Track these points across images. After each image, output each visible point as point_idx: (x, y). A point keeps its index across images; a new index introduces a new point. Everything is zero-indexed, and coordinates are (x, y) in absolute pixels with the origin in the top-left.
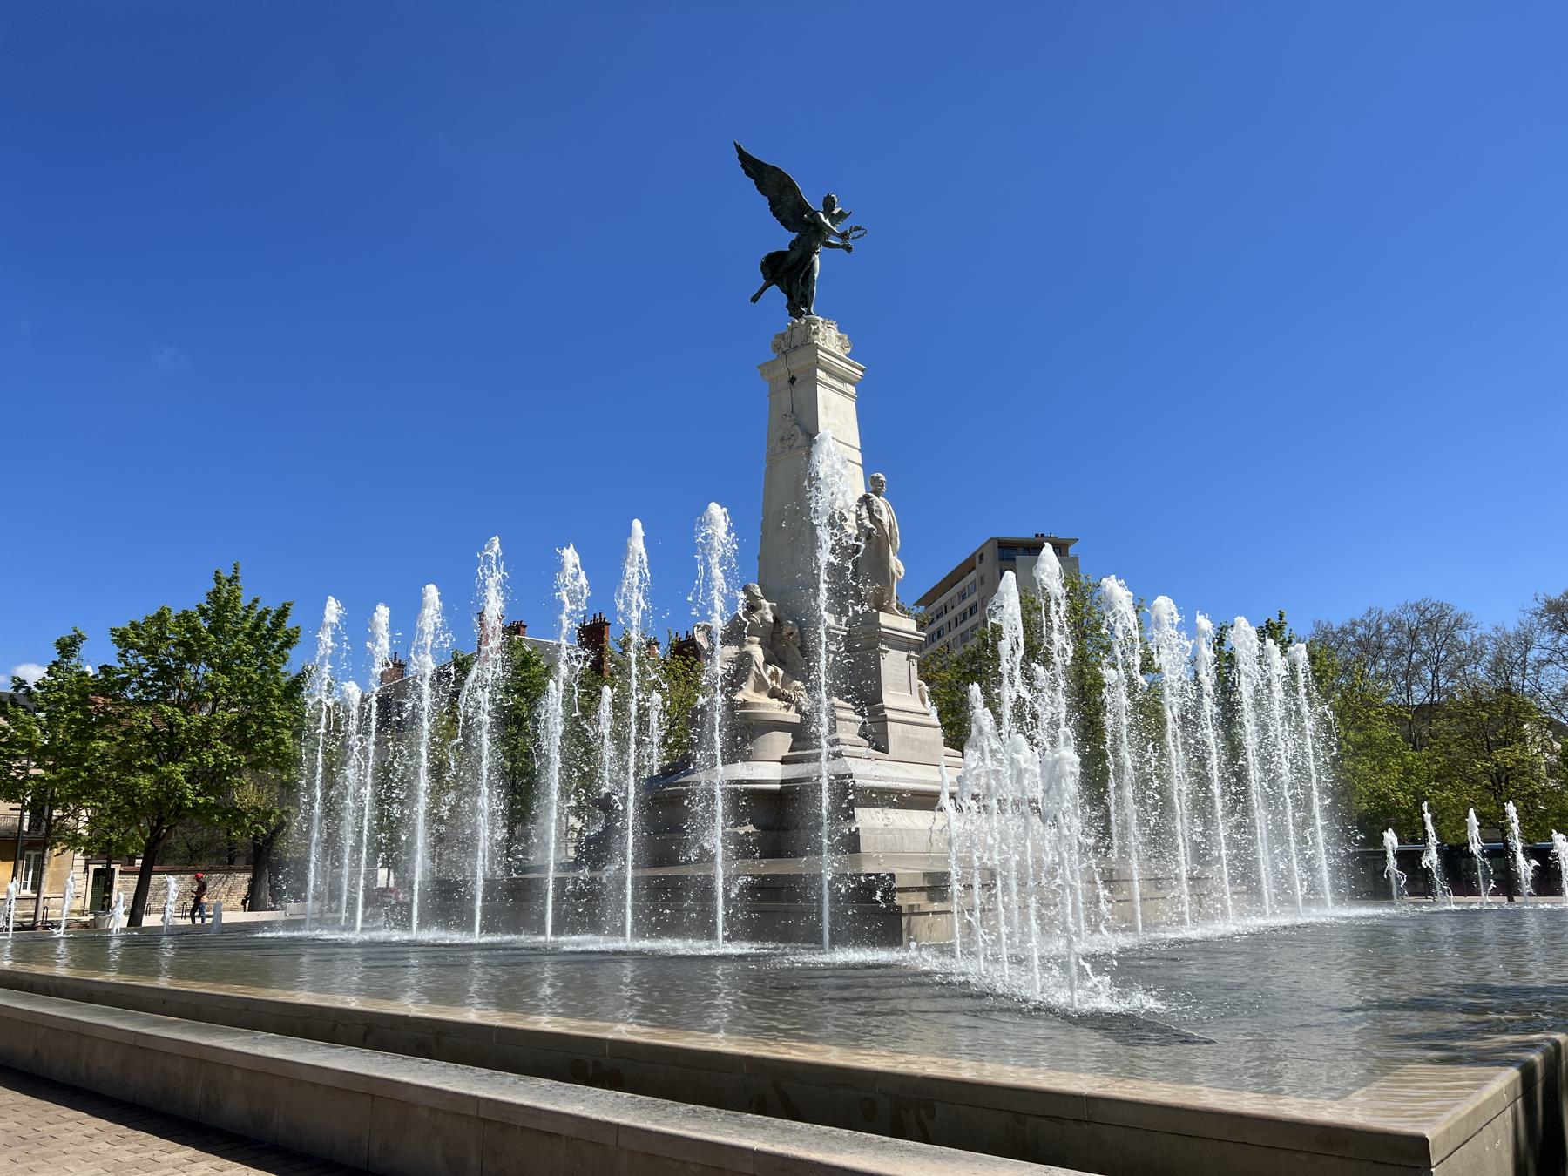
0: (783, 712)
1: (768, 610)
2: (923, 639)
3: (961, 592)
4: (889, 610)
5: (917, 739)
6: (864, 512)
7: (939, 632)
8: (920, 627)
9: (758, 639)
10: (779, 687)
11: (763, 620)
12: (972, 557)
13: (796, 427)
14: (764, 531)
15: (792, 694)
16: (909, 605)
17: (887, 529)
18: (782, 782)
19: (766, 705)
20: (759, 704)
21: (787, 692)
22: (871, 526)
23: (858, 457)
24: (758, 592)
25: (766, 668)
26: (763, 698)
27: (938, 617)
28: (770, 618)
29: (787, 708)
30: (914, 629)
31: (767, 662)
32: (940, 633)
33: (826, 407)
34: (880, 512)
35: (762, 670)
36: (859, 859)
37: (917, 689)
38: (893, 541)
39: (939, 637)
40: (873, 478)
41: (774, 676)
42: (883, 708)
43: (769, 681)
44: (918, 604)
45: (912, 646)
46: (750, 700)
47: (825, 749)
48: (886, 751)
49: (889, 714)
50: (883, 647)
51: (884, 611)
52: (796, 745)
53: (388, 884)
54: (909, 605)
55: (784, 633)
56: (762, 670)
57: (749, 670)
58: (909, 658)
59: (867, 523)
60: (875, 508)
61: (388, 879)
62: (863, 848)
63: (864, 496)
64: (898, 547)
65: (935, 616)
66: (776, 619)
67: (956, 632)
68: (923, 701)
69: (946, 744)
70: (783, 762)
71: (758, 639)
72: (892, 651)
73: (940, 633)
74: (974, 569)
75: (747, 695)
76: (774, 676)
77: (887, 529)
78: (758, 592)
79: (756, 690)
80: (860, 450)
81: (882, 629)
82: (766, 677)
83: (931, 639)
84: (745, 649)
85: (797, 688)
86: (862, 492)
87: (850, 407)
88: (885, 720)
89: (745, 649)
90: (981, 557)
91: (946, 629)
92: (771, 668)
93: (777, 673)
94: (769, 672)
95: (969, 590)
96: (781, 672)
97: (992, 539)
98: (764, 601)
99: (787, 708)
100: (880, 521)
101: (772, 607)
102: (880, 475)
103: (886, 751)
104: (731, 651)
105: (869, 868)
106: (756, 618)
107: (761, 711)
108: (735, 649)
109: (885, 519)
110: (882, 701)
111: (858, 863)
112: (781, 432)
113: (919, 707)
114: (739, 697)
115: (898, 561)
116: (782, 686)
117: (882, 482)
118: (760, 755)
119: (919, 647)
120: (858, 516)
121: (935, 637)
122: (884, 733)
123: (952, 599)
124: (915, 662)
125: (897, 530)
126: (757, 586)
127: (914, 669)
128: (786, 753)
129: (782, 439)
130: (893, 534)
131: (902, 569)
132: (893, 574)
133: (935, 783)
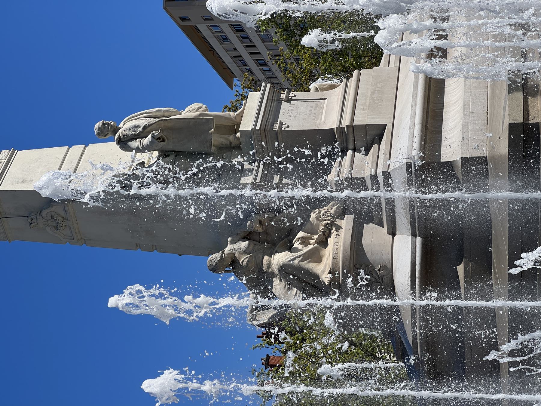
0: (342, 232)
1: (236, 246)
2: (269, 85)
3: (219, 41)
4: (238, 119)
5: (371, 95)
6: (135, 144)
7: (261, 64)
8: (255, 86)
9: (266, 258)
10: (316, 237)
11: (245, 252)
12: (183, 28)
13: (44, 213)
14: (153, 248)
15: (324, 223)
16: (230, 96)
17: (153, 120)
18: (414, 235)
19: (335, 251)
20: (334, 258)
21: (321, 228)
22: (150, 136)
23: (77, 149)
24: (216, 256)
25: (297, 250)
26: (328, 253)
27: (245, 65)
28: (244, 245)
29: (338, 228)
30: (258, 95)
31: (290, 248)
32: (262, 64)
33: (23, 182)
34: (136, 127)
35: (299, 254)
36: (493, 158)
37: (320, 93)
38: (166, 114)
39: (265, 64)
40: (99, 134)
41: (305, 241)
42: (339, 128)
43: (310, 247)
44: (231, 86)
45: (275, 97)
46: (329, 268)
47: (382, 194)
48: (385, 126)
49: (346, 122)
50: (276, 127)
51: (239, 125)
52: (376, 219)
53: (18, 151)
54: (230, 96)
55: (260, 230)
56: (299, 254)
57: (299, 269)
58: (288, 101)
59: (146, 141)
60: (131, 133)
61: (350, 264)
62: (481, 153)
63: (118, 143)
64: (172, 109)
65: (244, 68)
66: (244, 239)
67: (261, 47)
68: (333, 87)
69: (378, 66)
70: (393, 233)
71: (266, 258)
72: (281, 118)
73: (262, 64)
74: (195, 27)
75: (324, 271)
76: (305, 241)
77: (153, 120)
78: (216, 256)
79: (319, 260)
80: (70, 146)
81: (258, 127)
82: (306, 250)
83: (269, 75)
84: (276, 271)
85: (318, 218)
86: (113, 146)
87: (22, 156)
88: (352, 127)
89: (276, 271)
90: (184, 19)
91: (257, 57)
92: (297, 245)
93: (301, 238)
94: (300, 247)
95: (217, 32)
96: (301, 234)
97: (165, 8)
98: (227, 250)
99: (338, 228)
100: (145, 127)
101: (233, 242)
102: (96, 126)
103: (385, 126)
104: (278, 286)
105: (503, 148)
106: (243, 259)
107: (341, 248)
108: (276, 281)
109: (142, 122)
110: (332, 129)
111: (496, 159)
112: (48, 229)
113: (339, 90)
114: (326, 278)
115: (187, 109)
116: (317, 233)
117: (103, 125)
118: (385, 257)
119: (278, 88)
120: (138, 150)
121: (266, 68)
122: (365, 128)
123: (227, 51)
124: (292, 94)
125: (155, 110)
126: (210, 258)
127: (300, 95)
128: (385, 230)
129: (56, 228)
130: (158, 114)
131: (195, 106)
132: (200, 115)
133: (417, 78)
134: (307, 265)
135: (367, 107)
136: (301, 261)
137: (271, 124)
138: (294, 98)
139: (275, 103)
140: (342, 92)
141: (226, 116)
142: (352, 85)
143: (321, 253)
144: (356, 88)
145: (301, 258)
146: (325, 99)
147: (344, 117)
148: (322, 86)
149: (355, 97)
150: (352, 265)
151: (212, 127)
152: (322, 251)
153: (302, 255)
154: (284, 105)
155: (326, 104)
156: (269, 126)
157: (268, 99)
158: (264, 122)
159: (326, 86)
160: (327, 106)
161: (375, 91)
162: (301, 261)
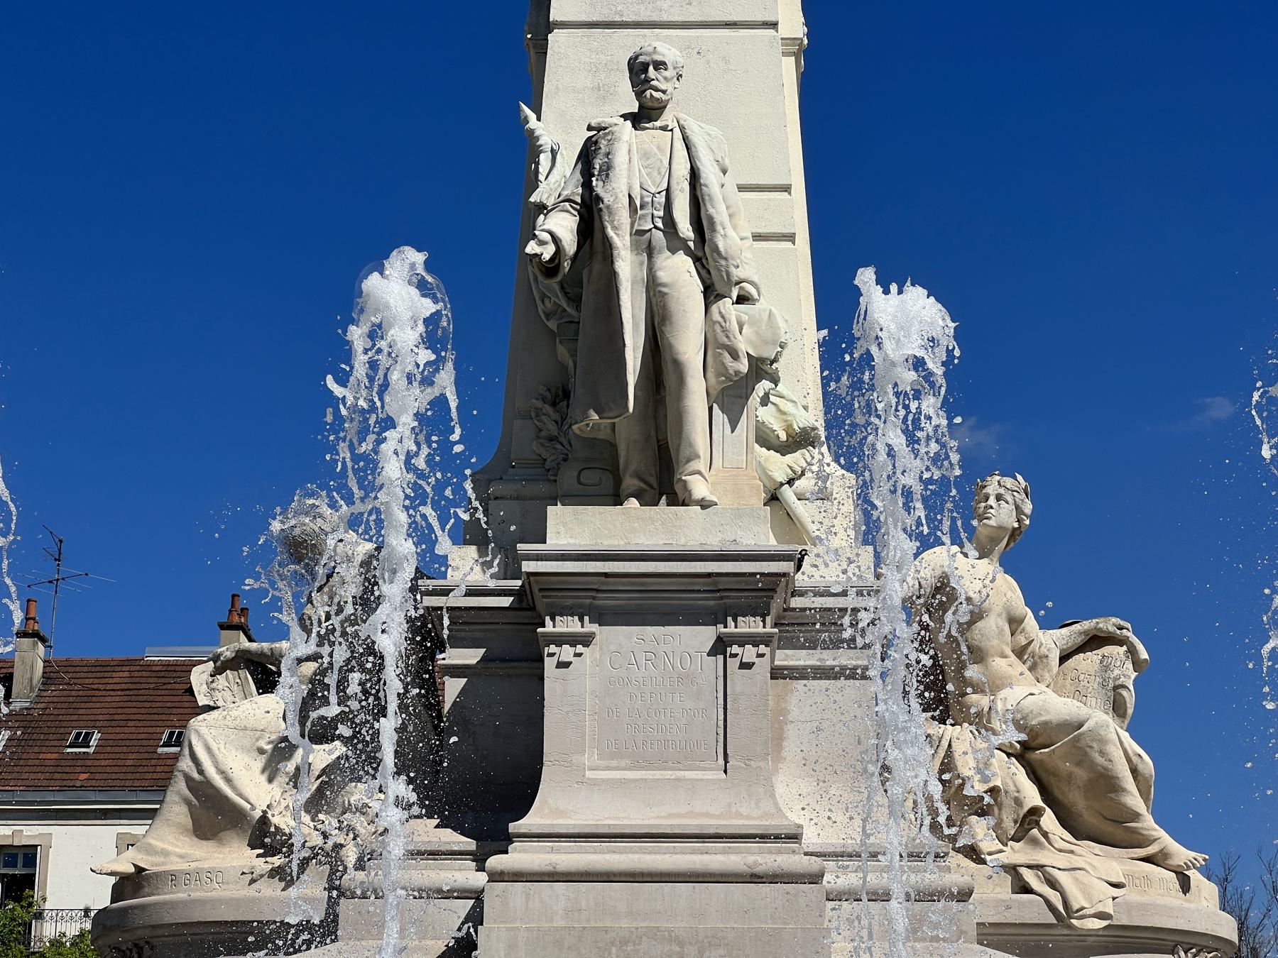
0: (271, 889)
20: (173, 875)
134: (177, 799)
135: (588, 921)
136: (188, 779)
137: (582, 606)
138: (733, 664)
139: (712, 603)
140: (718, 826)
141: (682, 447)
142: (720, 858)
143: (228, 832)
144: (614, 874)
145: (196, 775)
146: (725, 772)
147: (632, 847)
148: (1095, 745)
149: (642, 874)
150: (140, 933)
151: (606, 415)
152: (238, 834)
153: (205, 777)
154: (706, 635)
155: (710, 775)
156: (569, 602)
157: (709, 575)
158: (594, 583)
159: (1100, 760)
160: (678, 780)
161: (681, 944)
162: (188, 779)
